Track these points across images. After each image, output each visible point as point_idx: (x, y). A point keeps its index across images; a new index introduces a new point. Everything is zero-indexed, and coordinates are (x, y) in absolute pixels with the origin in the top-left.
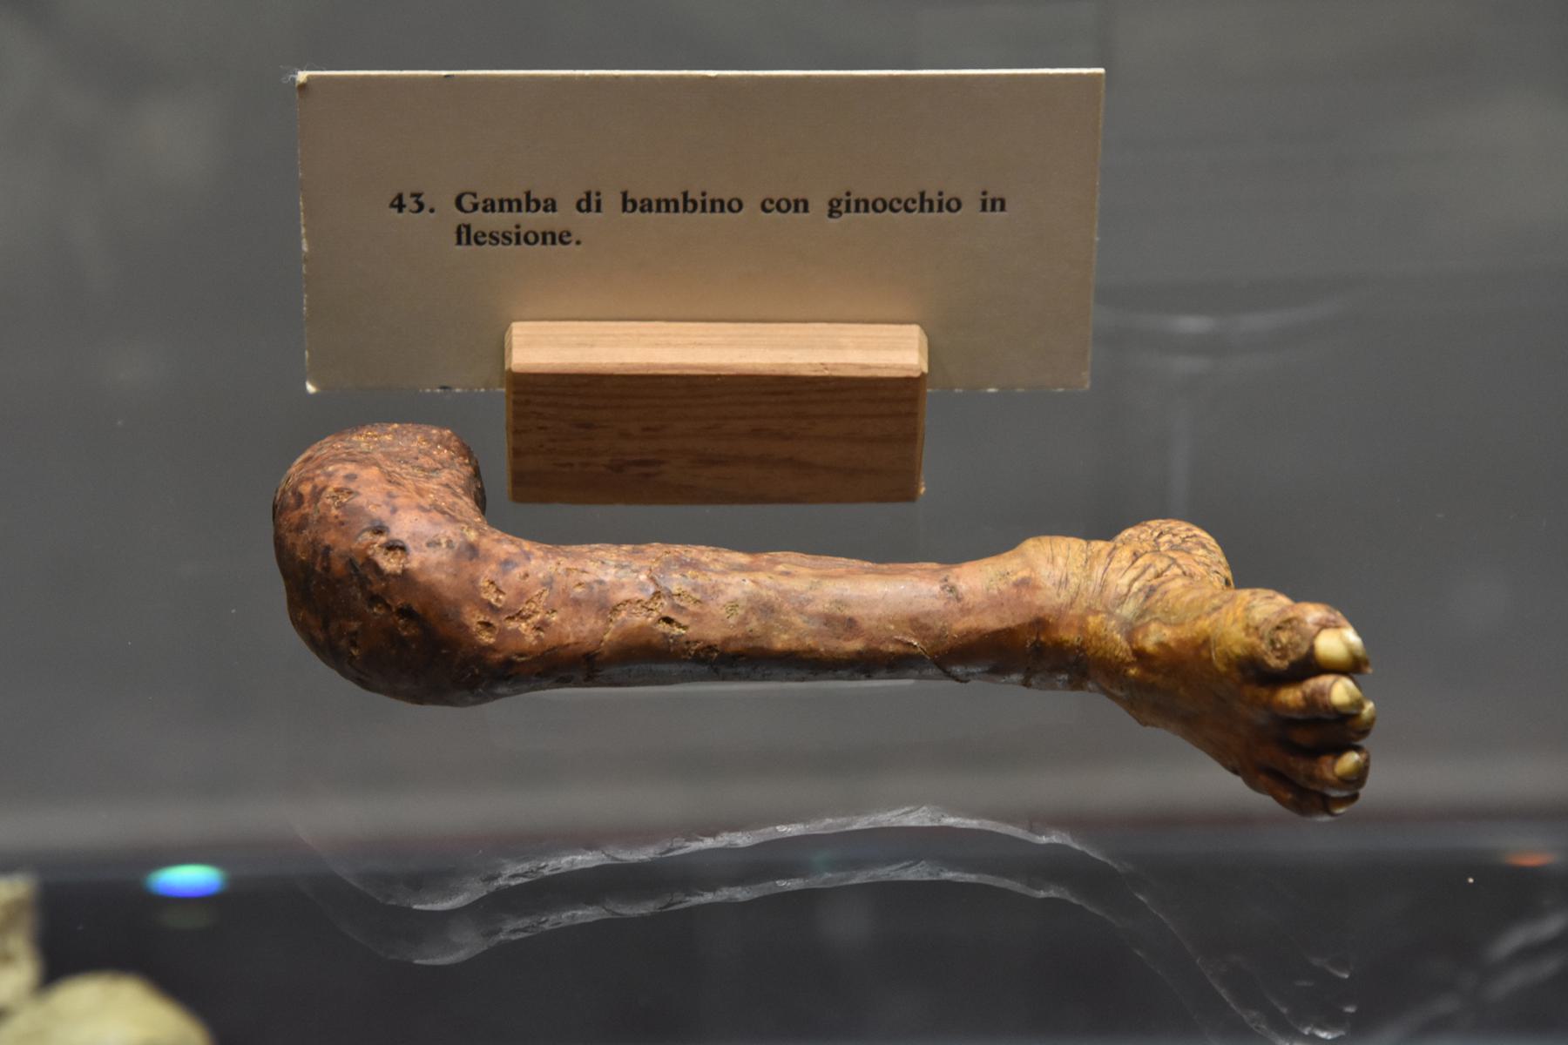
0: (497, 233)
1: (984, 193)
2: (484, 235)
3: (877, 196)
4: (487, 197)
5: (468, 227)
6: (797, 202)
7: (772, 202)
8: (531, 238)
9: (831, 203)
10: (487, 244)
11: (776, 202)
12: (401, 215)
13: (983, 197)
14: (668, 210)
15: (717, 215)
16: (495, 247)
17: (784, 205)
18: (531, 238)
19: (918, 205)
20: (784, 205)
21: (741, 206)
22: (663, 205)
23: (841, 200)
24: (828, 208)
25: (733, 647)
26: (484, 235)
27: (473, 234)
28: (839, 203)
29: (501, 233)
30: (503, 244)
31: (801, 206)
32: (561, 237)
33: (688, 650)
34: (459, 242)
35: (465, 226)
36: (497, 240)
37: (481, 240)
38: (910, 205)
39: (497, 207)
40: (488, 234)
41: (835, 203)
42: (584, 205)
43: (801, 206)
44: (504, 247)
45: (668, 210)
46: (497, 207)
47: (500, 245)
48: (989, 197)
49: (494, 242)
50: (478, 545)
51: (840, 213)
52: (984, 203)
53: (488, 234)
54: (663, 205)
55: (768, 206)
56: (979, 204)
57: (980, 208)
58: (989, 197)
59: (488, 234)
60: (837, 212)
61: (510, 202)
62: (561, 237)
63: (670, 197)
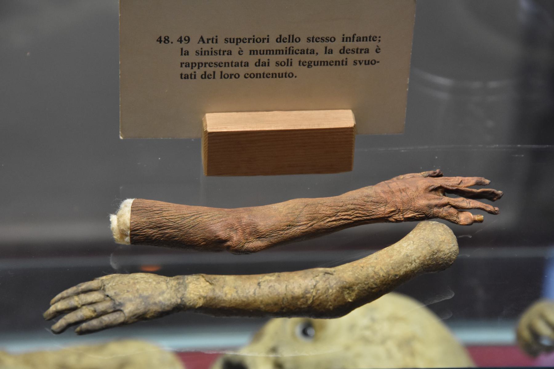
0: (324, 38)
1: (344, 35)
2: (350, 50)
3: (282, 61)
6: (257, 74)
7: (248, 74)
8: (259, 40)
10: (320, 42)
12: (160, 44)
13: (343, 37)
14: (270, 54)
15: (326, 67)
16: (328, 43)
17: (252, 76)
18: (259, 40)
20: (252, 76)
21: (239, 76)
22: (268, 52)
23: (312, 61)
26: (350, 50)
27: (294, 39)
28: (311, 62)
29: (325, 38)
30: (326, 42)
36: (324, 40)
37: (318, 40)
39: (362, 40)
40: (214, 63)
41: (310, 63)
44: (326, 43)
45: (270, 54)
46: (362, 40)
47: (325, 42)
48: (345, 36)
49: (323, 41)
51: (312, 66)
52: (343, 38)
53: (351, 49)
54: (268, 52)
55: (247, 76)
56: (342, 39)
57: (342, 40)
58: (345, 36)
59: (351, 49)
60: (310, 66)
61: (254, 51)
63: (280, 49)
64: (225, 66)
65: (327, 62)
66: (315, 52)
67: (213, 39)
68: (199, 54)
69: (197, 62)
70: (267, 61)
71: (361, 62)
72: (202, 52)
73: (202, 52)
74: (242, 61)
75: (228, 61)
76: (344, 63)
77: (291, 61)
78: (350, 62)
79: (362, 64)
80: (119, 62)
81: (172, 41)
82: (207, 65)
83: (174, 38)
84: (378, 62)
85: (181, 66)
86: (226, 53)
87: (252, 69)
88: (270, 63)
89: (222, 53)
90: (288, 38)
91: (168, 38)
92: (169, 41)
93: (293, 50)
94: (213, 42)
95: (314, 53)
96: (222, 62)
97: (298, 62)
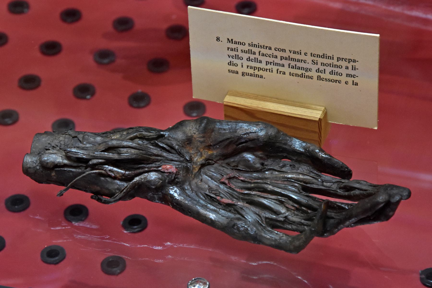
0: (327, 79)
2: (324, 79)
4: (298, 58)
5: (320, 76)
9: (242, 73)
10: (324, 81)
11: (278, 49)
19: (323, 72)
24: (242, 74)
25: (116, 202)
27: (239, 57)
31: (284, 51)
32: (311, 77)
33: (291, 145)
34: (318, 80)
35: (319, 76)
38: (270, 56)
41: (307, 69)
42: (331, 73)
43: (284, 51)
46: (237, 43)
50: (221, 125)
62: (311, 77)
64: (317, 57)
65: (351, 75)
66: (263, 77)
67: (270, 69)
68: (299, 53)
69: (257, 67)
70: (253, 73)
71: (291, 51)
72: (252, 44)
73: (252, 44)
74: (312, 53)
75: (292, 69)
76: (339, 59)
77: (355, 67)
78: (335, 59)
79: (291, 53)
80: (299, 279)
81: (222, 40)
82: (344, 60)
83: (273, 48)
84: (357, 61)
85: (248, 68)
86: (268, 48)
87: (240, 47)
88: (318, 63)
89: (265, 47)
90: (323, 70)
91: (219, 38)
92: (219, 40)
93: (233, 64)
94: (270, 71)
95: (262, 78)
96: (347, 58)
97: (289, 73)
